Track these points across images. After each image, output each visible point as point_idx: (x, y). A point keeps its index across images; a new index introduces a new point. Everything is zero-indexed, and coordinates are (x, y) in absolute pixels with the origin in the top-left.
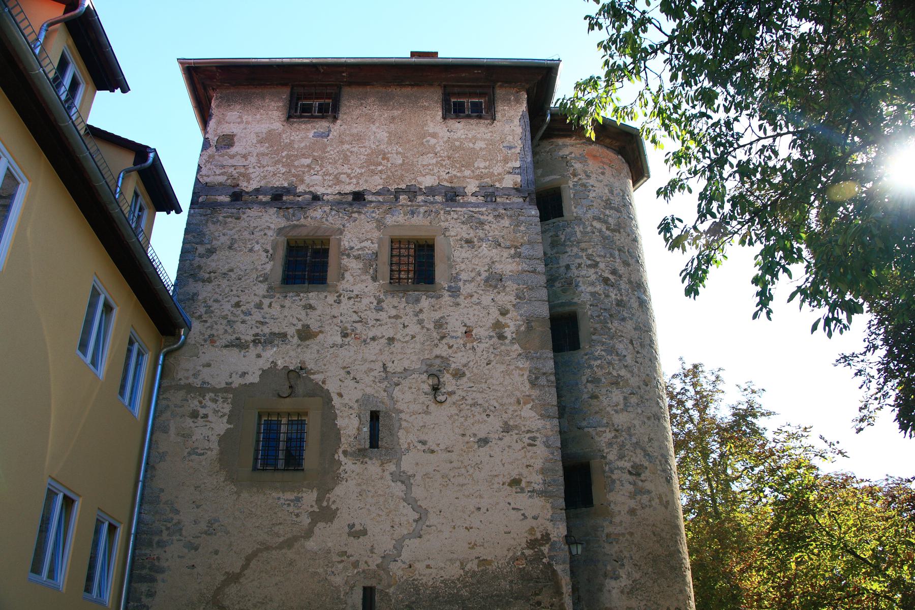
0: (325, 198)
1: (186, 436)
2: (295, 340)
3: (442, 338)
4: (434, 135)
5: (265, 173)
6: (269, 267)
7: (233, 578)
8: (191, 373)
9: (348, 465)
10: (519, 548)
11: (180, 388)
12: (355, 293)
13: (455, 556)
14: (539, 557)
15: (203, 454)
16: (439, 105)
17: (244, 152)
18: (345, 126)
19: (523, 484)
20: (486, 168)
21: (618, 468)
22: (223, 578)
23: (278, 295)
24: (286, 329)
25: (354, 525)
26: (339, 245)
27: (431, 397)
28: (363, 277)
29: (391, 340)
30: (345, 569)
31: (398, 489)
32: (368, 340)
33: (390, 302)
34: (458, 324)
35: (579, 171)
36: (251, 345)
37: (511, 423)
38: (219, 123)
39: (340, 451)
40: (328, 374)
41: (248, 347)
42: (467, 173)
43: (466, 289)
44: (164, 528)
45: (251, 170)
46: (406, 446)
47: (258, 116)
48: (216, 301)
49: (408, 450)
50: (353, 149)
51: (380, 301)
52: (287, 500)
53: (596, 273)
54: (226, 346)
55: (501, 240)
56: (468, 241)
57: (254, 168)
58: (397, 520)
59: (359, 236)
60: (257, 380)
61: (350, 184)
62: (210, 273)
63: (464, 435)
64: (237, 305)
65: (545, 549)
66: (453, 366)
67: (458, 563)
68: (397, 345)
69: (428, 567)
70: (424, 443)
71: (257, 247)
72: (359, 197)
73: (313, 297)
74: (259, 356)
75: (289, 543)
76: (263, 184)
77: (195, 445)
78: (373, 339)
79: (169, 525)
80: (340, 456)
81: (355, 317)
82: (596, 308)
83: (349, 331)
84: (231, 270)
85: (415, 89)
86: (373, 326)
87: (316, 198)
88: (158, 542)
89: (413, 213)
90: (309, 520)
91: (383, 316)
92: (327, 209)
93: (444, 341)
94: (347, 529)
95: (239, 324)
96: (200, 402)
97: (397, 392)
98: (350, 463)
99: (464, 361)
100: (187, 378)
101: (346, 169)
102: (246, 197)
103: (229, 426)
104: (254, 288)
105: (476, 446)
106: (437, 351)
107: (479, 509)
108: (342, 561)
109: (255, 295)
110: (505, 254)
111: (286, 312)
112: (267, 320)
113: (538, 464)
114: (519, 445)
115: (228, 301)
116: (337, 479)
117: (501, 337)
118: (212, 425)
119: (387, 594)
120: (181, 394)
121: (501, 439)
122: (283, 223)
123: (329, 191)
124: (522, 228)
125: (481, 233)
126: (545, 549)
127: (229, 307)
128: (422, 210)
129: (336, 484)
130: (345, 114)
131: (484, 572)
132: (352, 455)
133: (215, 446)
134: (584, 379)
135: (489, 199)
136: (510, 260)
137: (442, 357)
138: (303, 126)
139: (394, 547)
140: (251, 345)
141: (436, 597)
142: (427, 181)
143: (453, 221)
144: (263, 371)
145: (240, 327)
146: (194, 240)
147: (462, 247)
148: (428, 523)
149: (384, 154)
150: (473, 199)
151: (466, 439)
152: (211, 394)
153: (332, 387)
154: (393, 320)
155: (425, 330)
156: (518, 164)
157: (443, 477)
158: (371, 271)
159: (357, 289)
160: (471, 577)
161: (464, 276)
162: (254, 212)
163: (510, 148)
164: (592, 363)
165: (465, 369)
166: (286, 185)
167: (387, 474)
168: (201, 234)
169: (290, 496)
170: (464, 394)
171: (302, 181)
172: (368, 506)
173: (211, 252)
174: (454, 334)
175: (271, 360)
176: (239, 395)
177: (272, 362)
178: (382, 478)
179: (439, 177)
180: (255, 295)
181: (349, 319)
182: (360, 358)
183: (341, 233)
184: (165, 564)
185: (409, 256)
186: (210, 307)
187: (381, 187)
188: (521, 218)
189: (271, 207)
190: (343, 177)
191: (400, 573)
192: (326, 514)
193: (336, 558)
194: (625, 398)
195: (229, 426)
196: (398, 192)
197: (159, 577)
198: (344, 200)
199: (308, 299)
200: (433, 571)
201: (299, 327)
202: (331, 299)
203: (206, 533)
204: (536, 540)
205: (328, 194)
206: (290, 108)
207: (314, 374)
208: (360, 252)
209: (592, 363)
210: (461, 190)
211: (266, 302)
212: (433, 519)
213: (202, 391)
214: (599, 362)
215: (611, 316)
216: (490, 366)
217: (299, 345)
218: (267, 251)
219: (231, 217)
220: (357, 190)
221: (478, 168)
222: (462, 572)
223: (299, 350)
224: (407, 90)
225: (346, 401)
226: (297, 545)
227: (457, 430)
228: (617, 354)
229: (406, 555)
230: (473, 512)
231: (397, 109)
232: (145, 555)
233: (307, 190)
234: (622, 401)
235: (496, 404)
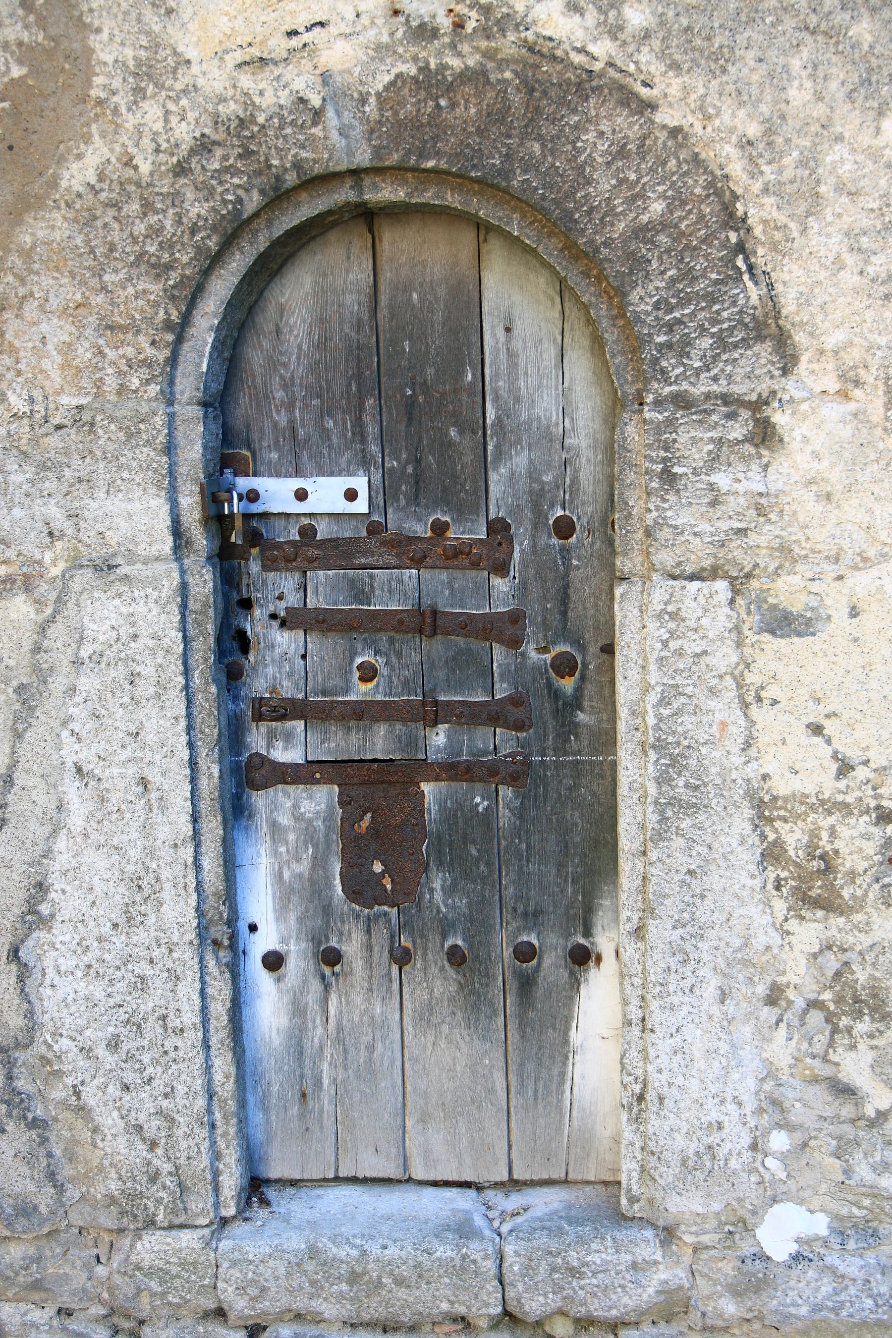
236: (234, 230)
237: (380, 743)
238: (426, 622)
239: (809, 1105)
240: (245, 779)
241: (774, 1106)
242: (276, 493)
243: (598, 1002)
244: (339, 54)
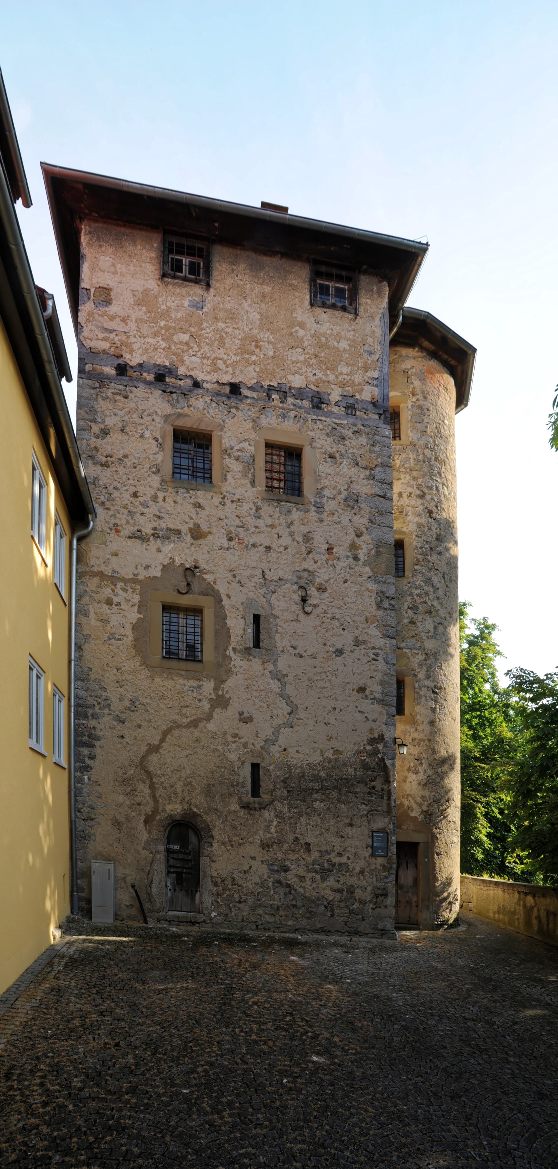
0: (205, 385)
1: (105, 621)
2: (188, 538)
3: (309, 552)
4: (302, 325)
5: (147, 346)
6: (160, 457)
7: (154, 749)
8: (102, 561)
9: (237, 662)
10: (362, 744)
11: (95, 574)
12: (237, 496)
13: (316, 745)
14: (376, 752)
15: (120, 640)
16: (307, 286)
17: (123, 314)
18: (218, 298)
19: (367, 692)
20: (348, 375)
21: (424, 686)
22: (147, 748)
23: (170, 490)
24: (180, 527)
25: (243, 713)
26: (221, 443)
27: (300, 607)
28: (243, 481)
29: (268, 548)
30: (238, 748)
31: (275, 685)
32: (250, 546)
33: (267, 509)
34: (322, 540)
35: (418, 391)
36: (151, 539)
37: (360, 638)
38: (93, 269)
39: (230, 648)
40: (218, 575)
41: (149, 540)
42: (332, 377)
43: (330, 505)
44: (95, 703)
45: (132, 340)
46: (281, 649)
47: (132, 268)
48: (116, 488)
49: (283, 651)
50: (227, 330)
51: (258, 509)
52: (191, 687)
53: (423, 504)
54: (130, 537)
55: (359, 459)
56: (331, 457)
57: (135, 337)
58: (275, 712)
59: (238, 435)
60: (159, 574)
61: (226, 372)
62: (106, 457)
63: (325, 644)
64: (135, 495)
65: (380, 746)
66: (318, 580)
67: (319, 751)
68: (273, 555)
69: (298, 752)
70: (295, 648)
71: (147, 434)
72: (235, 389)
73: (201, 496)
74: (159, 550)
75: (194, 724)
76: (145, 358)
77: (113, 631)
78: (254, 545)
79: (100, 700)
80: (230, 652)
81: (238, 522)
82: (420, 540)
83: (233, 535)
84: (126, 456)
85: (284, 260)
86: (253, 533)
87: (196, 384)
88: (93, 715)
89: (284, 417)
90: (209, 706)
91: (260, 523)
92: (208, 399)
93: (311, 556)
94: (238, 716)
95: (138, 515)
96: (113, 591)
97: (273, 598)
98: (238, 659)
99: (326, 577)
100: (99, 565)
101: (221, 353)
102: (130, 372)
103: (140, 616)
104: (149, 479)
105: (334, 656)
106: (305, 565)
107: (335, 709)
108: (235, 742)
109: (150, 486)
110: (362, 476)
111: (179, 508)
112: (163, 515)
113: (379, 676)
114: (365, 660)
115: (127, 490)
116: (229, 672)
117: (356, 558)
118: (126, 614)
119: (268, 770)
120: (96, 580)
121: (352, 652)
122: (168, 410)
123: (208, 378)
124: (377, 449)
125: (342, 449)
126: (380, 746)
127: (128, 496)
128: (292, 414)
129: (229, 677)
130: (218, 281)
131: (337, 760)
132: (239, 652)
133: (129, 632)
134: (406, 605)
135: (349, 412)
136: (365, 482)
137: (309, 571)
138: (178, 290)
139: (273, 734)
140: (151, 539)
141: (303, 776)
142: (297, 382)
143: (318, 432)
144: (164, 566)
145: (141, 520)
146: (87, 417)
147: (326, 462)
148: (298, 717)
149: (257, 342)
150: (335, 409)
151: (327, 648)
152: (121, 584)
153: (222, 588)
154: (269, 529)
155: (295, 543)
156: (376, 375)
157: (309, 679)
158: (250, 475)
159: (239, 493)
160: (328, 762)
161: (327, 493)
162: (140, 392)
163: (371, 353)
164: (413, 591)
165: (327, 585)
166: (167, 364)
167: (267, 672)
168: (93, 411)
169: (195, 683)
170: (325, 608)
171: (182, 361)
172: (253, 698)
173: (105, 432)
174: (319, 550)
175: (170, 555)
176: (146, 586)
177: (171, 558)
178: (263, 675)
179: (306, 378)
180: (150, 486)
181: (233, 523)
182: (243, 563)
183: (222, 430)
184: (101, 734)
185: (292, 466)
186: (111, 494)
187: (255, 381)
188: (377, 437)
189: (156, 388)
190: (220, 364)
191: (277, 755)
192: (221, 702)
193: (230, 739)
194: (435, 628)
195: (140, 616)
196: (271, 389)
197: (97, 743)
198: (222, 391)
199: (197, 497)
200: (301, 756)
201: (191, 525)
202: (217, 500)
203: (129, 709)
204: (374, 738)
205: (207, 382)
206: (164, 263)
207: (206, 573)
208: (239, 453)
209: (413, 591)
210: (326, 397)
211: (161, 495)
212: (301, 714)
213: (113, 579)
214: (419, 591)
215: (431, 548)
216: (346, 584)
217: (192, 544)
218: (156, 439)
219: (120, 394)
220: (233, 381)
221: (341, 374)
222: (321, 758)
223: (193, 549)
224: (276, 261)
225: (234, 603)
226: (201, 725)
227: (320, 640)
228: (433, 586)
229: (282, 741)
230: (330, 712)
231: (267, 284)
232: (83, 724)
233: (188, 374)
234: (432, 630)
235: (349, 620)
236: (170, 824)
237: (179, 870)
238: (183, 860)
239: (215, 903)
240: (169, 872)
241: (212, 904)
242: (171, 847)
243: (198, 895)
244: (178, 811)
